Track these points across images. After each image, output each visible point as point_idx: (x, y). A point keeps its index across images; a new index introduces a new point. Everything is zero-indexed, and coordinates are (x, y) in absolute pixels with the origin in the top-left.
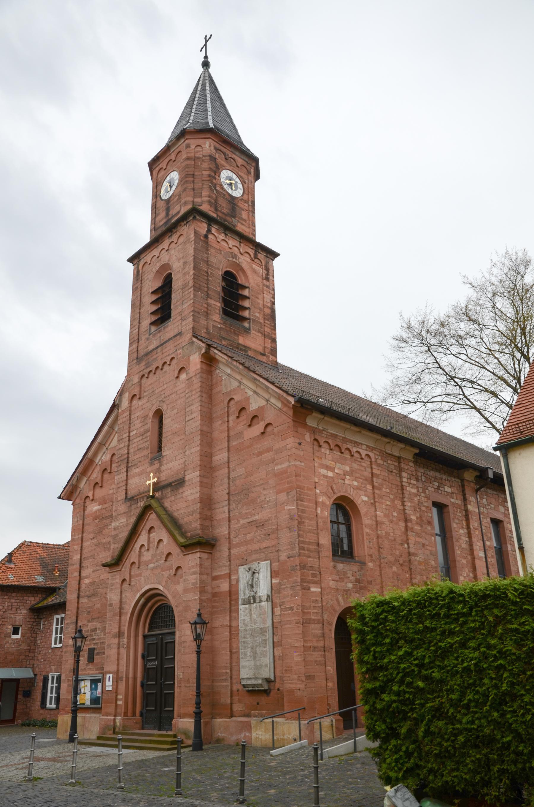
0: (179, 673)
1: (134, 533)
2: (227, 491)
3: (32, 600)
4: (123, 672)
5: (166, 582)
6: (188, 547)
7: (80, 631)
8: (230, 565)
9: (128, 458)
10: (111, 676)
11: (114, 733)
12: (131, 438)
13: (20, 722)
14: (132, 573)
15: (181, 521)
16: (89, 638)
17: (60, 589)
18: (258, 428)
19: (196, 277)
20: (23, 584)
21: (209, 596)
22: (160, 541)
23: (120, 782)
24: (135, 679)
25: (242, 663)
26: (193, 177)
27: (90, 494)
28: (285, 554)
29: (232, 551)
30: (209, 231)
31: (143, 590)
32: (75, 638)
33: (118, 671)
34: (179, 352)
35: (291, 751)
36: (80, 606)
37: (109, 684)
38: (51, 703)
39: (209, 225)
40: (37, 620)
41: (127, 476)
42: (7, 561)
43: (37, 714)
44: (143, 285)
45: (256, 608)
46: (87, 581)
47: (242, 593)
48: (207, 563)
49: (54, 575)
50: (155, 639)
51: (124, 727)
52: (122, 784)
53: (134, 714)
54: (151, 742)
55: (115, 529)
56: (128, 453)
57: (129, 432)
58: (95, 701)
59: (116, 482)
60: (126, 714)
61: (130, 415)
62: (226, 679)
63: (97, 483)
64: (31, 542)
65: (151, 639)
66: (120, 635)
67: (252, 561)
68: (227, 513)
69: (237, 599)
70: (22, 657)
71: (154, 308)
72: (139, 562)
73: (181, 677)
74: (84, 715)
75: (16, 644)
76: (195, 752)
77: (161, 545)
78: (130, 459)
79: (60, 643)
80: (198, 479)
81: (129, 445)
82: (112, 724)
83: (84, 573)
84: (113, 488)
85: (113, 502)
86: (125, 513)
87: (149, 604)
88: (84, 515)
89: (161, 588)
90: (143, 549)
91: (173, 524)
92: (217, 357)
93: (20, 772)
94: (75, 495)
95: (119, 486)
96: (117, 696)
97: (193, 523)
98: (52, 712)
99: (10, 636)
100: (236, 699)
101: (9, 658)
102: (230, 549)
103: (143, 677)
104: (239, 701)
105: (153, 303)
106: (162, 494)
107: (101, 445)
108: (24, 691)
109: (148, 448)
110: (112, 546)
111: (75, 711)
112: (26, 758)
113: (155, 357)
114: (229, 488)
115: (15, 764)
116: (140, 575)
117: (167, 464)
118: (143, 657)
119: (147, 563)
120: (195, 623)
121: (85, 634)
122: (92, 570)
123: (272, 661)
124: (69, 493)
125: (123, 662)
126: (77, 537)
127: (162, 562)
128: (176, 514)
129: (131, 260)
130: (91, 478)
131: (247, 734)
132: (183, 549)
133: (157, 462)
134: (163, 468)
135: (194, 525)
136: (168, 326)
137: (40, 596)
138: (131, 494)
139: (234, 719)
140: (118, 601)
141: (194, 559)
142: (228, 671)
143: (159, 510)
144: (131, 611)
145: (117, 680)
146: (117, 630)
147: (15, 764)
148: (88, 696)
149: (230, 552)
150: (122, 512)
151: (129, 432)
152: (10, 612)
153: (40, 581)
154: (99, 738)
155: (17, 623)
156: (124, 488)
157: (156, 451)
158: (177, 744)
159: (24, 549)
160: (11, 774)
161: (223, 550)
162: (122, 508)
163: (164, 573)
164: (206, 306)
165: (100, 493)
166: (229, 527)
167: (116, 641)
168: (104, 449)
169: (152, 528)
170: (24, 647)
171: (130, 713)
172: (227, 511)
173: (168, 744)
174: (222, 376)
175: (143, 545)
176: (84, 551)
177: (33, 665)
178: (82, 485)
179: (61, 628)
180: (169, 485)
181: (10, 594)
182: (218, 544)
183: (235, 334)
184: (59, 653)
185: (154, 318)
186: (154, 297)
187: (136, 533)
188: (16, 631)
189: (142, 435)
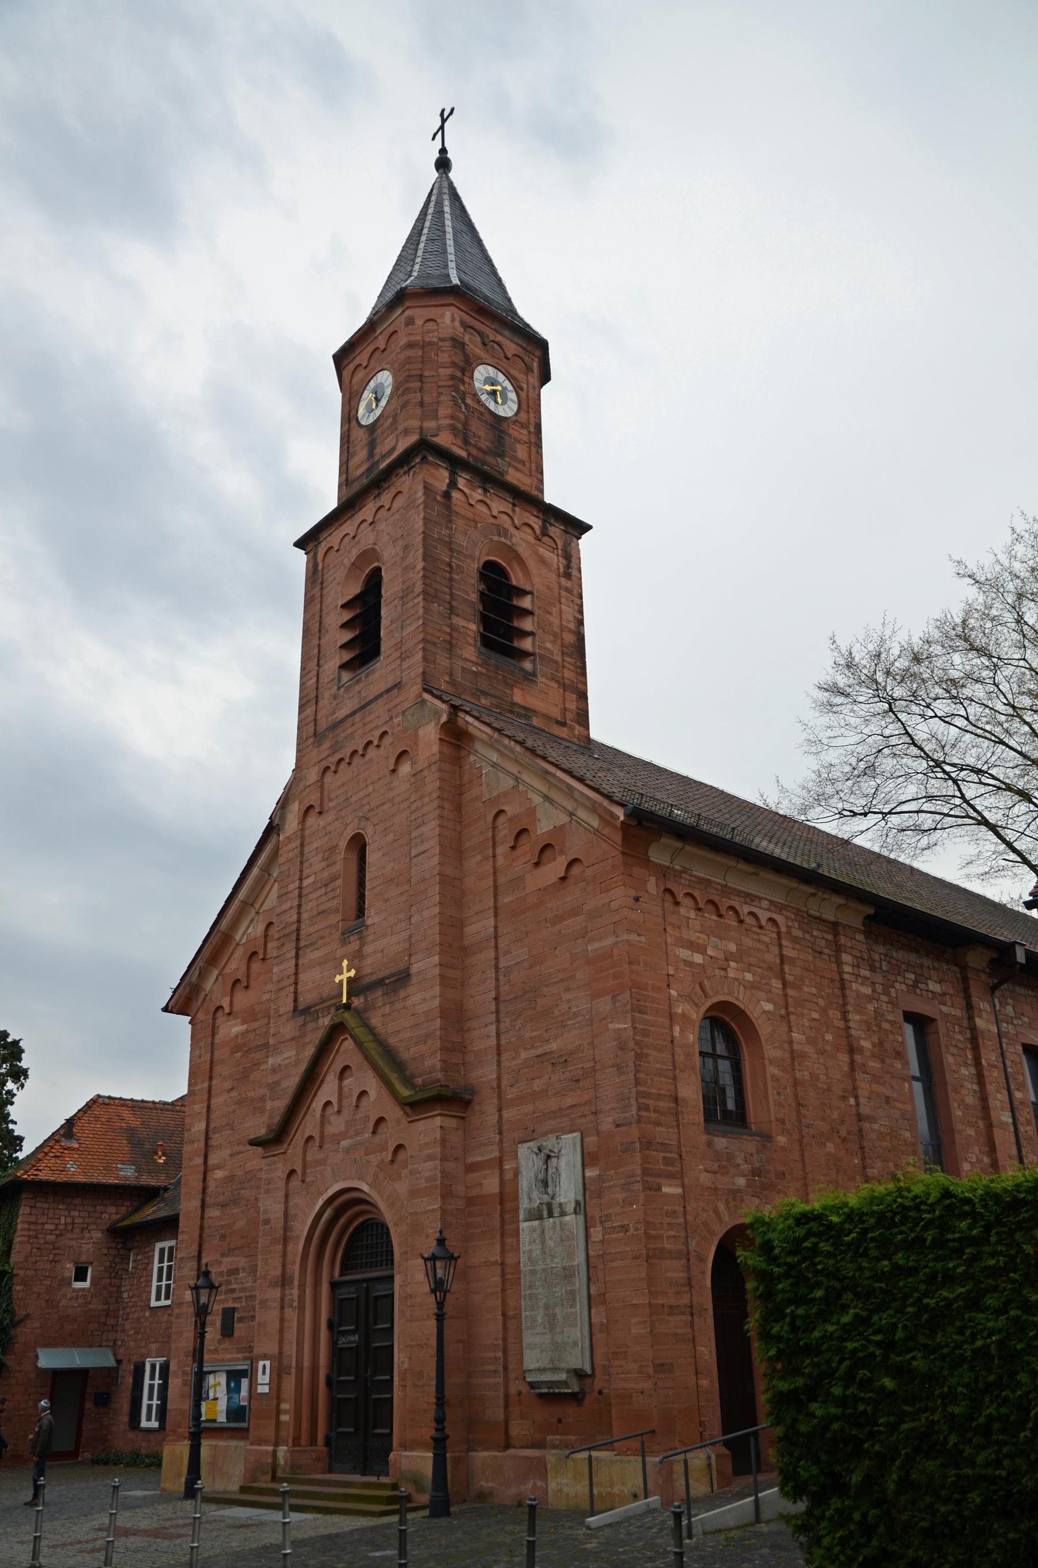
0: (400, 1358)
2: (493, 994)
3: (112, 1213)
5: (376, 1176)
6: (416, 1106)
8: (501, 1141)
9: (298, 930)
10: (268, 1363)
11: (274, 1479)
12: (305, 892)
13: (88, 1455)
16: (223, 1288)
18: (555, 868)
19: (428, 574)
20: (95, 1181)
22: (363, 1093)
25: (528, 1338)
26: (421, 381)
27: (225, 1003)
28: (610, 1119)
29: (506, 1114)
30: (453, 484)
31: (330, 1192)
32: (196, 1288)
33: (281, 1353)
34: (396, 721)
36: (206, 1224)
37: (264, 1382)
38: (149, 1419)
39: (453, 474)
40: (121, 1252)
41: (296, 965)
42: (64, 1136)
44: (325, 591)
46: (219, 1174)
47: (525, 1197)
49: (155, 1162)
50: (353, 1289)
51: (294, 1467)
53: (313, 1441)
54: (347, 1498)
55: (274, 1071)
56: (299, 921)
57: (301, 879)
58: (236, 1413)
60: (296, 1441)
61: (302, 845)
62: (495, 1371)
63: (237, 981)
64: (110, 1098)
66: (284, 1281)
67: (545, 1134)
68: (494, 1038)
69: (517, 1209)
71: (347, 636)
73: (406, 1366)
74: (214, 1442)
75: (81, 1300)
76: (436, 1520)
77: (364, 1102)
78: (302, 933)
79: (167, 1298)
80: (437, 971)
81: (299, 906)
82: (270, 1460)
83: (213, 1160)
86: (293, 1039)
87: (342, 1221)
88: (213, 1043)
89: (365, 1188)
90: (329, 1111)
91: (388, 1061)
92: (471, 729)
93: (88, 1558)
95: (281, 985)
96: (278, 1405)
97: (428, 1061)
99: (70, 1284)
102: (500, 1110)
105: (345, 626)
106: (366, 1000)
107: (246, 905)
109: (337, 911)
111: (197, 1435)
113: (349, 731)
114: (497, 987)
115: (79, 1542)
116: (323, 1162)
117: (374, 941)
118: (331, 1325)
120: (434, 1258)
122: (229, 1151)
123: (586, 1334)
124: (182, 1001)
125: (291, 1335)
126: (199, 1087)
127: (367, 1135)
128: (392, 1041)
129: (300, 544)
130: (227, 971)
131: (539, 1484)
132: (408, 1109)
133: (356, 937)
134: (368, 949)
135: (428, 1063)
136: (374, 671)
138: (302, 1004)
139: (511, 1451)
140: (281, 1214)
141: (432, 1126)
142: (500, 1354)
143: (360, 1032)
144: (305, 1233)
145: (278, 1374)
146: (278, 1272)
147: (79, 1542)
148: (222, 1405)
149: (500, 1116)
150: (288, 1037)
151: (301, 879)
152: (69, 1235)
153: (127, 1173)
154: (243, 1489)
155: (84, 1258)
156: (292, 989)
157: (353, 917)
158: (400, 1504)
159: (97, 1110)
161: (487, 1112)
162: (289, 1029)
163: (372, 1157)
164: (448, 630)
165: (243, 999)
166: (499, 1065)
167: (277, 1293)
169: (346, 1068)
170: (97, 1305)
171: (304, 1441)
173: (381, 1503)
174: (480, 768)
175: (328, 1103)
176: (214, 1115)
177: (115, 1341)
178: (209, 984)
179: (170, 1268)
180: (380, 983)
183: (506, 683)
184: (166, 1317)
185: (347, 656)
186: (347, 616)
188: (80, 1275)
189: (326, 885)
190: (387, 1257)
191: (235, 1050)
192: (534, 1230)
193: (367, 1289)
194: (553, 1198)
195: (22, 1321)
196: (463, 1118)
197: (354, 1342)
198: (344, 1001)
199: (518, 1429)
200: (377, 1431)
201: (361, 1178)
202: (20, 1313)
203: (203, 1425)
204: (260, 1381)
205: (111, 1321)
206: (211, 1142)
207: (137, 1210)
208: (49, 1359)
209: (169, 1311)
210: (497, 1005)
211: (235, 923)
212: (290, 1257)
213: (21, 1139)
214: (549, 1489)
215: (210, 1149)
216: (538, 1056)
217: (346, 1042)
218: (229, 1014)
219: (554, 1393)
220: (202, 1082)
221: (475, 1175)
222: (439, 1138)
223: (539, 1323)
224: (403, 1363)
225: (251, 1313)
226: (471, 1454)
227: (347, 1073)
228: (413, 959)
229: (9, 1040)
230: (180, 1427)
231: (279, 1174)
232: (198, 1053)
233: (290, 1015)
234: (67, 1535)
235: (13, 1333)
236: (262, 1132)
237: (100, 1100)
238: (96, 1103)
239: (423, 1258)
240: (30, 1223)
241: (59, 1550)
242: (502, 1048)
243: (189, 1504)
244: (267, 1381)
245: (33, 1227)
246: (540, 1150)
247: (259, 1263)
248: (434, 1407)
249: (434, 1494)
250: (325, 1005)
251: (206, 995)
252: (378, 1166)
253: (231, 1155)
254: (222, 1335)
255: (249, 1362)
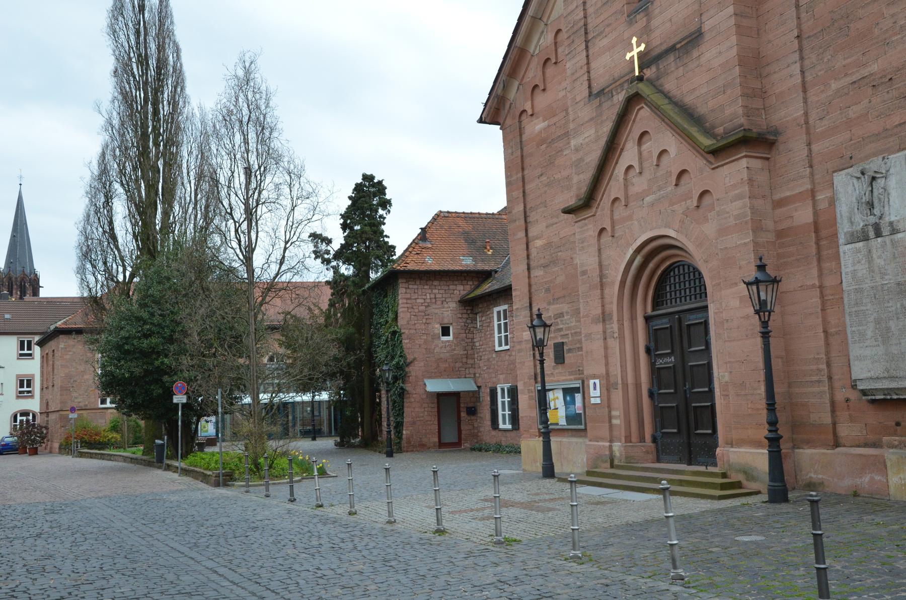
0: (720, 374)
1: (611, 148)
2: (796, 33)
3: (461, 290)
4: (616, 375)
5: (682, 222)
6: (719, 153)
7: (539, 316)
8: (812, 174)
9: (585, 25)
10: (597, 381)
11: (612, 466)
13: (467, 445)
14: (615, 217)
15: (701, 110)
16: (552, 328)
17: (496, 272)
20: (446, 269)
21: (771, 237)
22: (663, 152)
23: (675, 567)
24: (638, 386)
25: (855, 351)
27: (528, 107)
29: (815, 148)
31: (639, 242)
32: (533, 327)
33: (607, 374)
35: (380, 425)
36: (533, 282)
38: (504, 423)
40: (471, 316)
41: (587, 56)
42: (421, 240)
43: (487, 435)
45: (884, 245)
46: (539, 243)
47: (846, 221)
48: (762, 178)
49: (485, 253)
50: (665, 320)
51: (629, 459)
52: (680, 571)
53: (642, 439)
54: (681, 483)
55: (577, 150)
56: (585, 17)
58: (573, 418)
59: (569, 72)
60: (628, 439)
62: (819, 382)
63: (536, 86)
64: (448, 212)
65: (659, 322)
66: (604, 318)
67: (867, 157)
69: (835, 235)
70: (458, 365)
72: (627, 197)
73: (727, 379)
74: (559, 439)
75: (448, 348)
76: (778, 506)
77: (665, 160)
78: (590, 27)
79: (506, 344)
80: (732, 21)
82: (607, 453)
83: (533, 232)
84: (566, 88)
85: (567, 110)
86: (591, 119)
87: (651, 265)
88: (521, 142)
89: (672, 233)
90: (632, 173)
91: (687, 119)
93: (480, 524)
94: (503, 113)
95: (574, 78)
96: (610, 412)
97: (728, 110)
98: (508, 434)
99: (439, 338)
100: (843, 415)
101: (443, 366)
102: (809, 144)
103: (652, 383)
104: (852, 419)
106: (658, 69)
107: (536, 19)
108: (467, 408)
110: (575, 179)
111: (547, 431)
112: (486, 500)
114: (799, 26)
115: (472, 510)
116: (630, 218)
117: (661, 13)
118: (648, 350)
119: (641, 197)
120: (757, 282)
121: (548, 322)
122: (545, 224)
124: (493, 113)
125: (615, 359)
126: (514, 178)
127: (671, 188)
128: (688, 100)
130: (526, 80)
132: (711, 158)
133: (642, 14)
134: (655, 23)
135: (728, 112)
137: (471, 283)
138: (596, 88)
139: (839, 449)
140: (596, 266)
141: (738, 170)
142: (824, 366)
143: (656, 98)
144: (619, 278)
145: (608, 388)
146: (599, 311)
147: (472, 510)
148: (562, 412)
149: (810, 150)
150: (586, 119)
152: (434, 306)
153: (467, 263)
154: (589, 473)
155: (446, 321)
156: (586, 77)
158: (731, 487)
159: (440, 221)
160: (468, 527)
161: (794, 149)
162: (586, 113)
163: (676, 207)
165: (542, 101)
166: (805, 101)
167: (599, 328)
168: (542, 25)
169: (644, 133)
170: (459, 351)
171: (635, 437)
172: (798, 71)
173: (715, 488)
175: (630, 167)
176: (529, 199)
177: (475, 374)
178: (512, 94)
179: (506, 324)
180: (672, 49)
181: (430, 283)
182: (781, 139)
184: (507, 357)
187: (615, 149)
188: (445, 331)
190: (701, 291)
191: (542, 142)
192: (858, 251)
193: (680, 320)
194: (880, 218)
195: (411, 362)
196: (768, 159)
197: (671, 362)
198: (637, 74)
199: (844, 431)
200: (698, 432)
201: (667, 226)
202: (410, 358)
203: (551, 427)
204: (592, 395)
205: (470, 361)
206: (529, 220)
207: (477, 287)
208: (434, 386)
209: (509, 353)
210: (800, 43)
211: (528, 38)
212: (607, 299)
213: (394, 247)
214: (890, 483)
215: (529, 225)
216: (855, 82)
217: (642, 111)
218: (532, 115)
219: (892, 400)
220: (517, 173)
221: (784, 209)
222: (746, 178)
223: (868, 337)
224: (723, 376)
225: (578, 345)
226: (797, 450)
227: (646, 138)
228: (704, 18)
229: (375, 181)
230: (531, 428)
231: (591, 233)
232: (510, 151)
233: (587, 100)
234: (461, 504)
235: (407, 369)
236: (572, 202)
237: (442, 215)
238: (440, 218)
239: (745, 283)
240: (407, 299)
241: (457, 516)
242: (807, 85)
243: (548, 482)
244: (598, 395)
245: (409, 301)
246: (863, 173)
247: (581, 306)
248: (765, 411)
249: (771, 484)
250: (618, 83)
251: (511, 104)
252: (683, 213)
253: (547, 227)
254: (556, 362)
255: (580, 382)
